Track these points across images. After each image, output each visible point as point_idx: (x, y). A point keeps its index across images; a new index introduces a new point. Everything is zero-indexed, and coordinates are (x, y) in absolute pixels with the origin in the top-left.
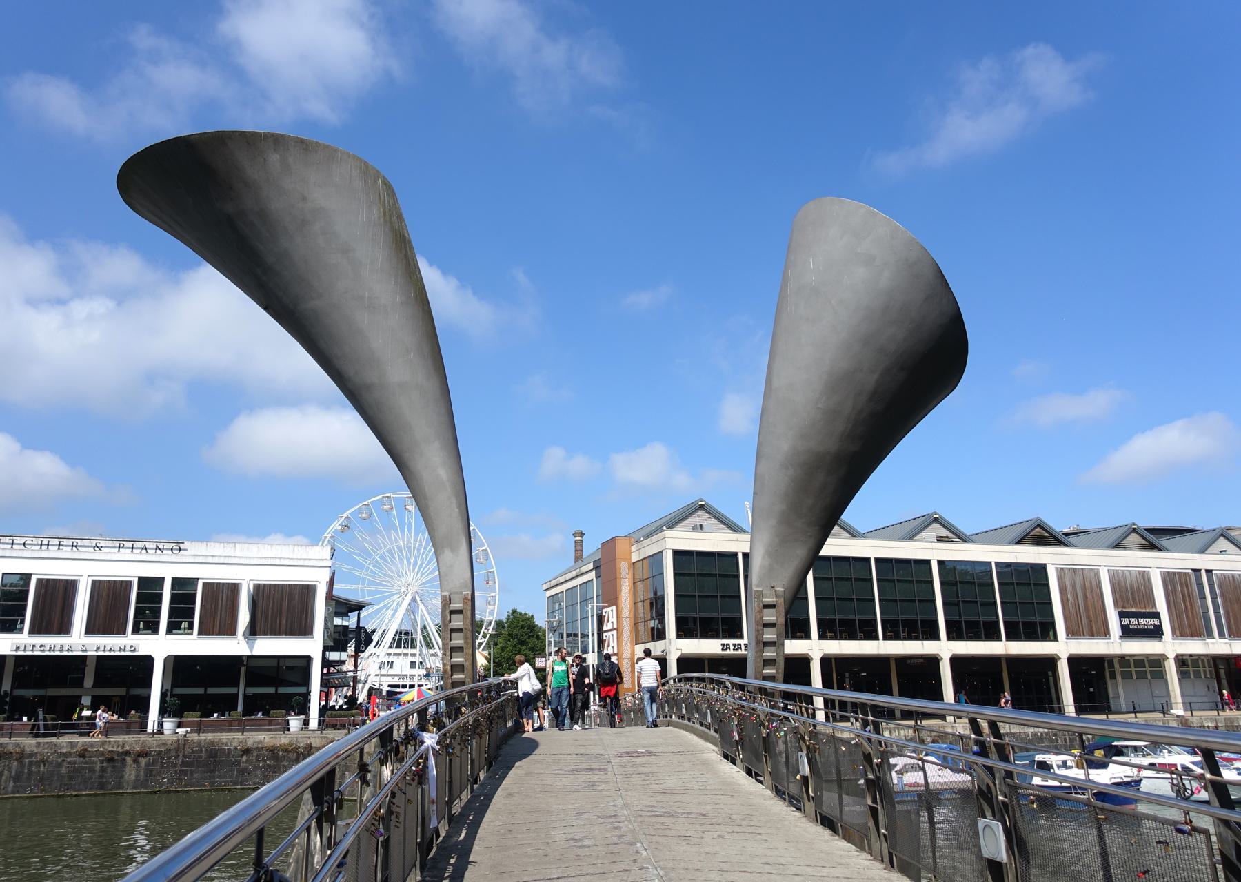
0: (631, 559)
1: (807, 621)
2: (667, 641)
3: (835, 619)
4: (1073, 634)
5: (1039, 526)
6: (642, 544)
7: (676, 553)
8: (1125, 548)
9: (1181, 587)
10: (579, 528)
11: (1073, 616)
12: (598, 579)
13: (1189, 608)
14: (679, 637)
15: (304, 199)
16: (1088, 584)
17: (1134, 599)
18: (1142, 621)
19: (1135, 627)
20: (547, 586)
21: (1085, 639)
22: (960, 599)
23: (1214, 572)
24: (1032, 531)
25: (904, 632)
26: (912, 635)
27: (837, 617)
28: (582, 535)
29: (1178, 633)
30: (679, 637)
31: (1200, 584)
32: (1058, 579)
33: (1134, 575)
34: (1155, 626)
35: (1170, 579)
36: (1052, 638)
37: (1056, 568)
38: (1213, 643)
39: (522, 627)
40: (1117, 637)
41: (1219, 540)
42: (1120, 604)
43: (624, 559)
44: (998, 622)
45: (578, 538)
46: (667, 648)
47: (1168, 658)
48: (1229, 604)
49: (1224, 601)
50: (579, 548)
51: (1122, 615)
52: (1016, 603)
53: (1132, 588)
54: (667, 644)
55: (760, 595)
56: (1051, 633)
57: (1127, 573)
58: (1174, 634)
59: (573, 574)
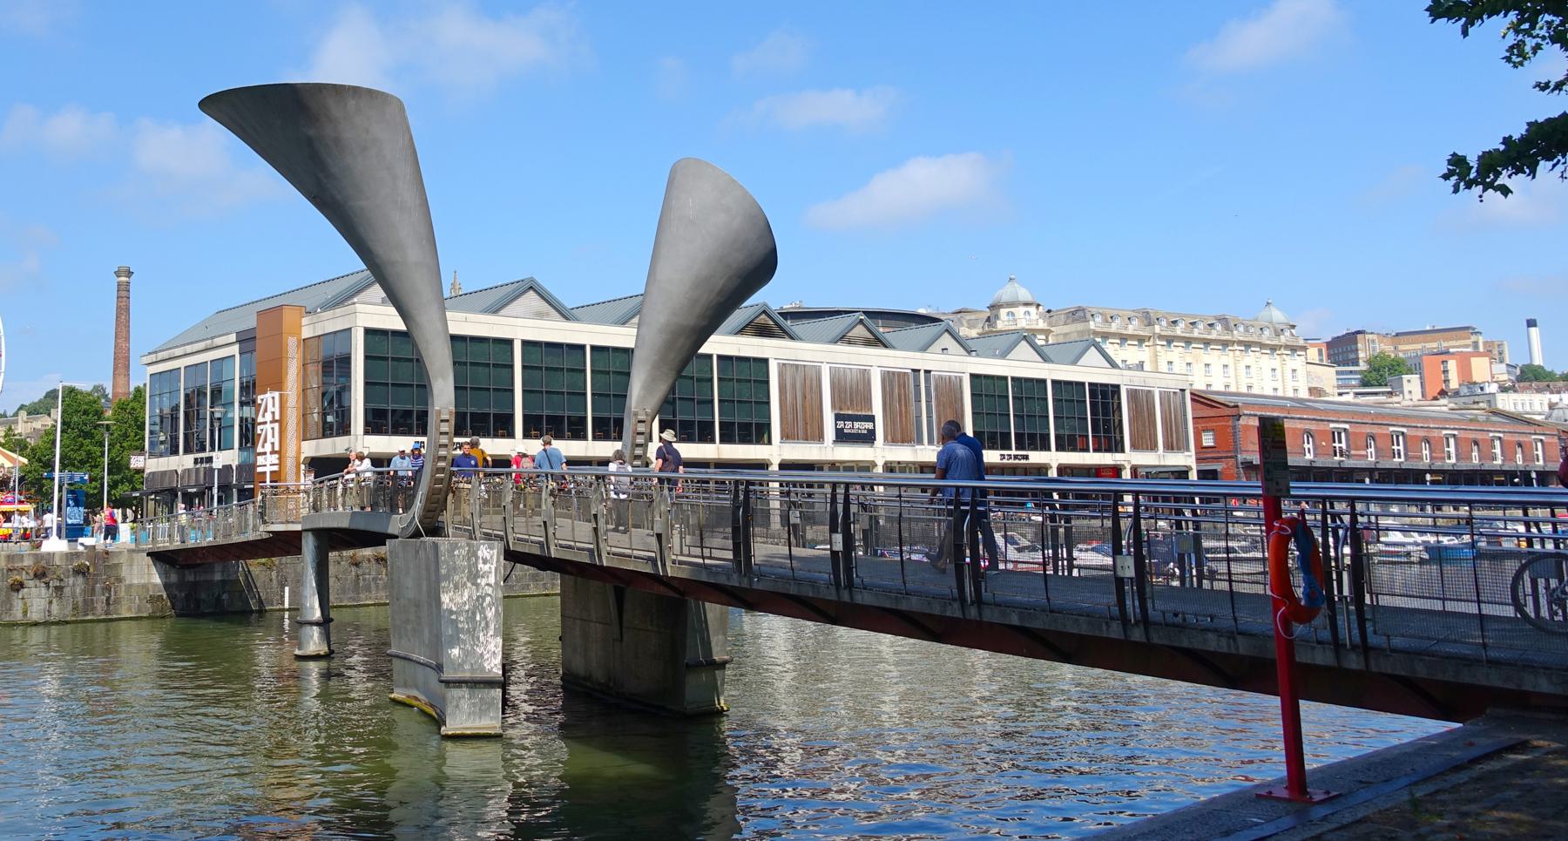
0: (300, 334)
1: (511, 417)
2: (352, 437)
3: (490, 414)
4: (788, 438)
5: (764, 312)
6: (319, 317)
7: (369, 332)
8: (849, 343)
9: (899, 386)
10: (125, 264)
11: (790, 417)
12: (243, 356)
13: (903, 412)
14: (366, 432)
15: (367, 131)
16: (808, 382)
17: (852, 401)
18: (857, 425)
19: (849, 431)
20: (153, 358)
21: (1147, 467)
22: (677, 396)
23: (932, 373)
24: (757, 317)
25: (614, 432)
26: (745, 439)
27: (492, 412)
28: (129, 273)
29: (889, 438)
30: (366, 432)
31: (917, 386)
32: (779, 376)
33: (854, 374)
34: (868, 430)
35: (890, 379)
36: (766, 441)
37: (779, 364)
38: (921, 450)
39: (86, 413)
40: (831, 441)
41: (943, 336)
42: (837, 406)
43: (292, 335)
44: (713, 423)
45: (124, 279)
46: (352, 446)
47: (876, 465)
48: (942, 408)
49: (938, 406)
50: (124, 294)
51: (838, 417)
52: (733, 401)
53: (851, 388)
54: (352, 441)
55: (636, 414)
56: (766, 436)
57: (848, 371)
58: (886, 439)
59: (201, 346)
